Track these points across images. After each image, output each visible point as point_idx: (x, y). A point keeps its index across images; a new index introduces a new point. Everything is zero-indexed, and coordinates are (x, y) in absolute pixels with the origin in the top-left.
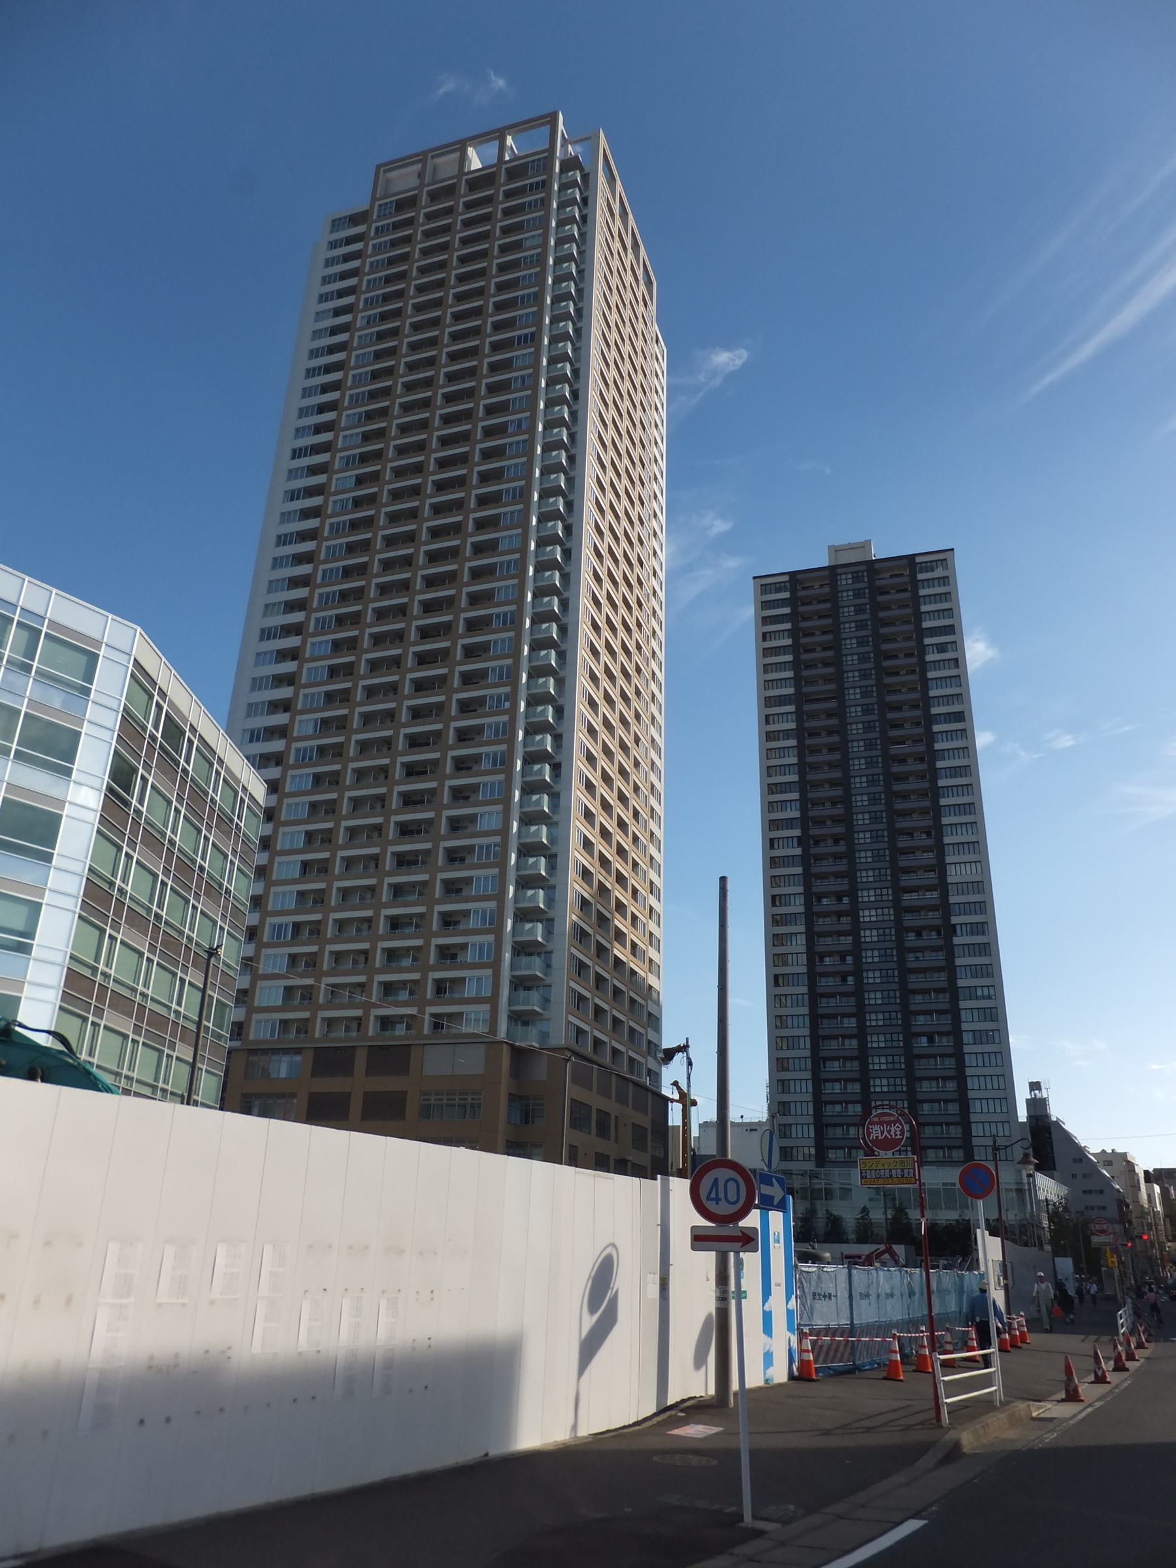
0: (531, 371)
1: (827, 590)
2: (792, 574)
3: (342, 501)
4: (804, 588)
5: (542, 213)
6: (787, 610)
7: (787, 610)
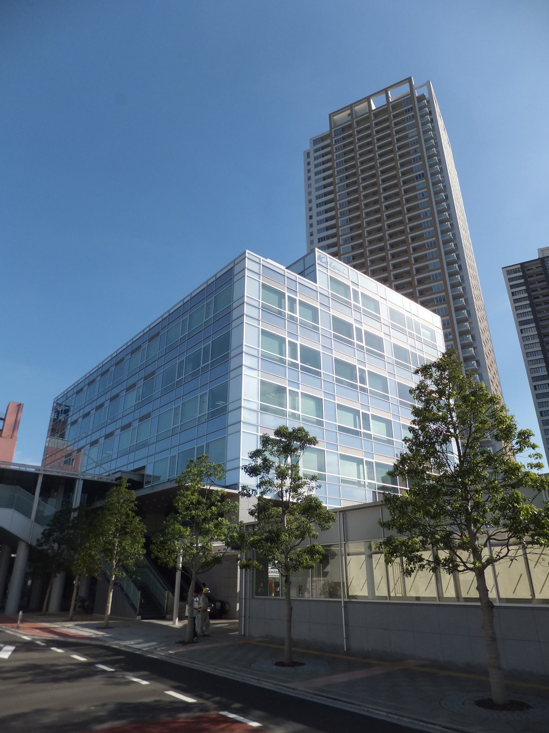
0: (426, 189)
1: (541, 269)
2: (522, 264)
3: (347, 257)
4: (528, 270)
5: (414, 121)
6: (522, 281)
7: (522, 281)
